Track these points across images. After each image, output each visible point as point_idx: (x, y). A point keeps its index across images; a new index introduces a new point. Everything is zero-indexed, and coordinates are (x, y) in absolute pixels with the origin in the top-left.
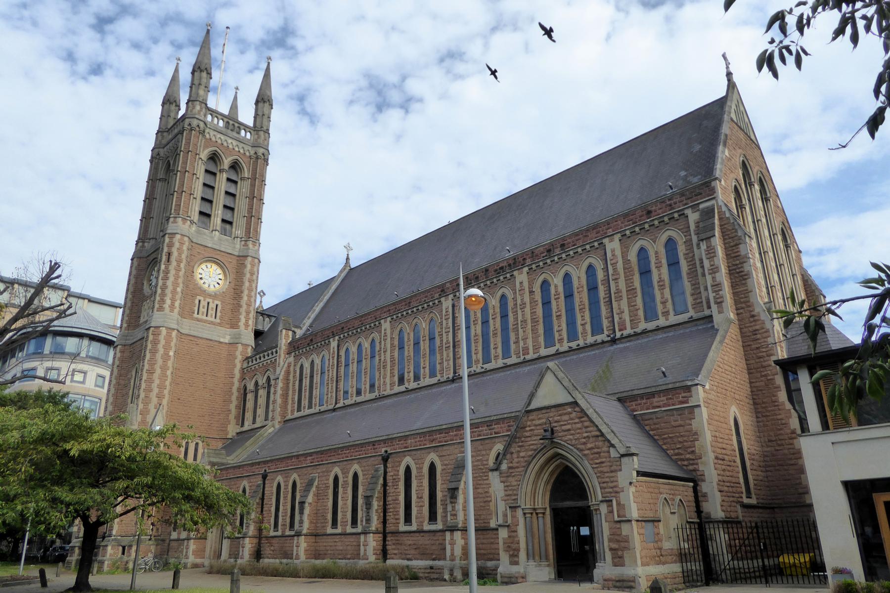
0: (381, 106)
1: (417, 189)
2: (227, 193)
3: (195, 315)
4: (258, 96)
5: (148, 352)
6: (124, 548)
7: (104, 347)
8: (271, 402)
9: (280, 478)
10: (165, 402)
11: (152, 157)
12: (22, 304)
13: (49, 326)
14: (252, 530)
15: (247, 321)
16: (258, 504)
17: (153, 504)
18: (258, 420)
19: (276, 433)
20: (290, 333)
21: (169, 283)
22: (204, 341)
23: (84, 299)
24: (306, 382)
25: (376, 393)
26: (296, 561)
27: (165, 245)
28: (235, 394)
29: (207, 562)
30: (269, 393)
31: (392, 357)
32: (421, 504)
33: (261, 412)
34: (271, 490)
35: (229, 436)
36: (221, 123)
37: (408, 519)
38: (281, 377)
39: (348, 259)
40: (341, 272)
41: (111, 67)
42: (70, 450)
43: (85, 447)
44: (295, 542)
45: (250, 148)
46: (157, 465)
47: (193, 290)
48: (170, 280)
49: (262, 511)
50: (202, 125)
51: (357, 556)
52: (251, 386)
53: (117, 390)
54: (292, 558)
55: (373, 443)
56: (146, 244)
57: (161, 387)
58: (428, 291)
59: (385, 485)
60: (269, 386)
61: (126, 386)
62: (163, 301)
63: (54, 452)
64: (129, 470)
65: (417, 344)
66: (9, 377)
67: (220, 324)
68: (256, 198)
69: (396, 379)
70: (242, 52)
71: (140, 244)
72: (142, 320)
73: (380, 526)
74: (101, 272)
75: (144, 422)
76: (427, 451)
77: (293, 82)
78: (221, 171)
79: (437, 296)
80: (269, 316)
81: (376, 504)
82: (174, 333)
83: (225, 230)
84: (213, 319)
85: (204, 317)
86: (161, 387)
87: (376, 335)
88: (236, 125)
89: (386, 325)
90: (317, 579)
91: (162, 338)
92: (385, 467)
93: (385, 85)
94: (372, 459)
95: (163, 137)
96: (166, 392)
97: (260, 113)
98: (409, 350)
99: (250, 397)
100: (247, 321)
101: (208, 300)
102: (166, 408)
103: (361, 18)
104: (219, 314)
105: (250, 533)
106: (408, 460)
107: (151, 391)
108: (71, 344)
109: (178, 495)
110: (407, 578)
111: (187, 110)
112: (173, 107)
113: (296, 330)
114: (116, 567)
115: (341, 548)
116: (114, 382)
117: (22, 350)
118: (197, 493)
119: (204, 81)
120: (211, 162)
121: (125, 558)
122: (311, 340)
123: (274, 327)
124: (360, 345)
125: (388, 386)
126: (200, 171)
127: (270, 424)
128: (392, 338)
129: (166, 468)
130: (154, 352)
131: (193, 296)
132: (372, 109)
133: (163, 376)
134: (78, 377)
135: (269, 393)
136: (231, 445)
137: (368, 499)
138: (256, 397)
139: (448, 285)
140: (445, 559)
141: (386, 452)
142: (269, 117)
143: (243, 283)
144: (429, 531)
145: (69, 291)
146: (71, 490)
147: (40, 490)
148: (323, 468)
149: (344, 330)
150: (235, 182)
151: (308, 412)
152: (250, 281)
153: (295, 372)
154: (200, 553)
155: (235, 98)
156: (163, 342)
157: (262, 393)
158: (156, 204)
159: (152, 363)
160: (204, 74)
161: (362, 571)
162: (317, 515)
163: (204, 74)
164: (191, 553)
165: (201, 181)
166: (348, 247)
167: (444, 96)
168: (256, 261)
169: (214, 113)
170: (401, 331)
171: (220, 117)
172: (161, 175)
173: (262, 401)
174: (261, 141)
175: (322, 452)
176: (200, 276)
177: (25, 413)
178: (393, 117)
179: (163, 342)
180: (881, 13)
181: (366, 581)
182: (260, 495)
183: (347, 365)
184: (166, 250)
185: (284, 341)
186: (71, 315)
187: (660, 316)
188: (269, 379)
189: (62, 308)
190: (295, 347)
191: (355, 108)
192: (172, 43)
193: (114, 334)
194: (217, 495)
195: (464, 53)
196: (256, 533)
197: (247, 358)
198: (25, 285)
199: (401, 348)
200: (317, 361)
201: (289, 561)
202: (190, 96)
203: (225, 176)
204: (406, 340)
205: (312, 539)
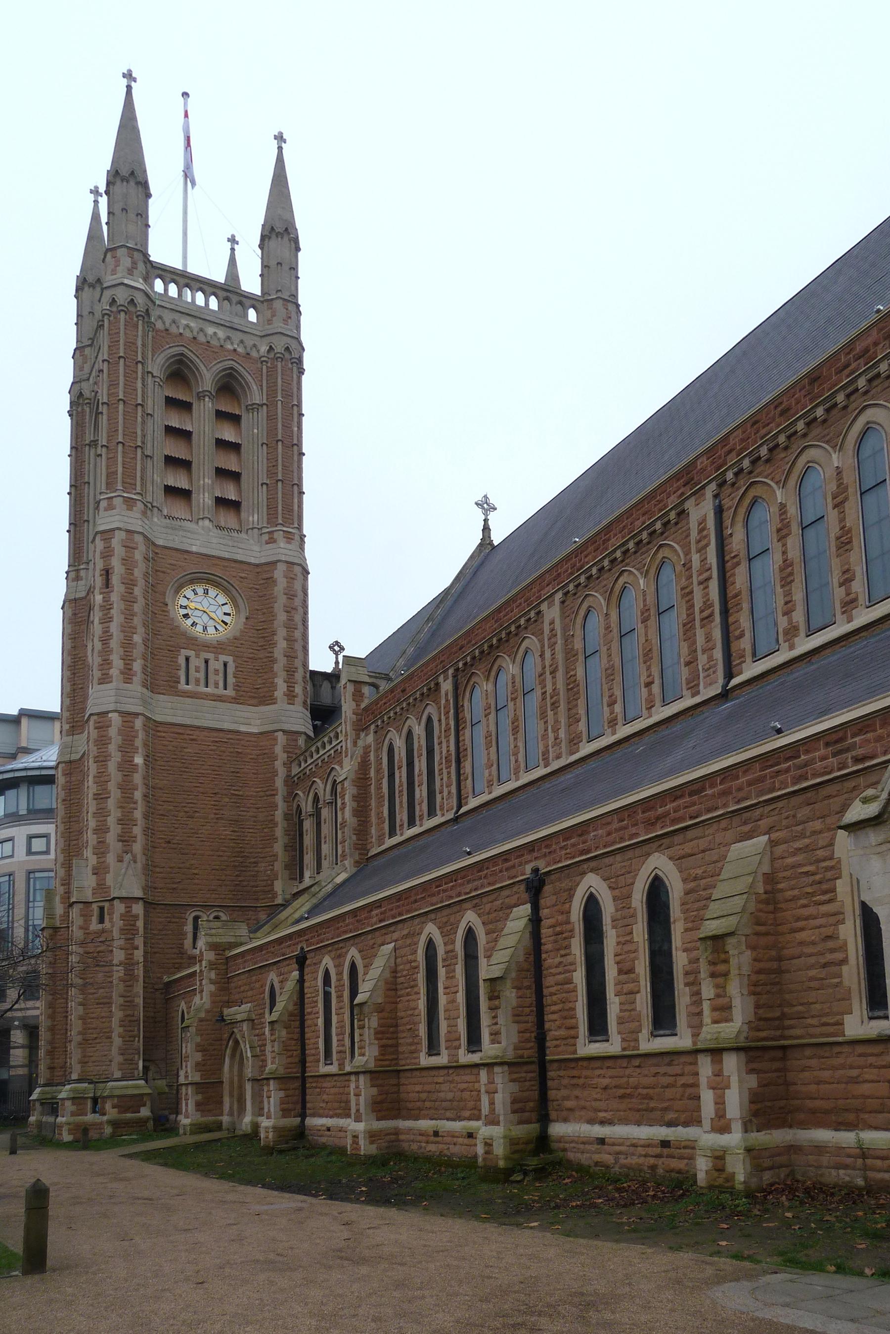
3: (183, 686)
24: (401, 776)
32: (627, 987)
37: (598, 1027)
39: (486, 529)
44: (353, 1086)
50: (140, 299)
52: (307, 807)
67: (235, 700)
78: (200, 397)
85: (202, 689)
96: (137, 831)
99: (308, 825)
102: (140, 858)
104: (231, 680)
106: (592, 882)
107: (120, 821)
115: (450, 1096)
131: (174, 650)
138: (319, 824)
140: (698, 1122)
141: (536, 871)
166: (486, 506)
168: (297, 569)
176: (184, 612)
180: (563, 1332)
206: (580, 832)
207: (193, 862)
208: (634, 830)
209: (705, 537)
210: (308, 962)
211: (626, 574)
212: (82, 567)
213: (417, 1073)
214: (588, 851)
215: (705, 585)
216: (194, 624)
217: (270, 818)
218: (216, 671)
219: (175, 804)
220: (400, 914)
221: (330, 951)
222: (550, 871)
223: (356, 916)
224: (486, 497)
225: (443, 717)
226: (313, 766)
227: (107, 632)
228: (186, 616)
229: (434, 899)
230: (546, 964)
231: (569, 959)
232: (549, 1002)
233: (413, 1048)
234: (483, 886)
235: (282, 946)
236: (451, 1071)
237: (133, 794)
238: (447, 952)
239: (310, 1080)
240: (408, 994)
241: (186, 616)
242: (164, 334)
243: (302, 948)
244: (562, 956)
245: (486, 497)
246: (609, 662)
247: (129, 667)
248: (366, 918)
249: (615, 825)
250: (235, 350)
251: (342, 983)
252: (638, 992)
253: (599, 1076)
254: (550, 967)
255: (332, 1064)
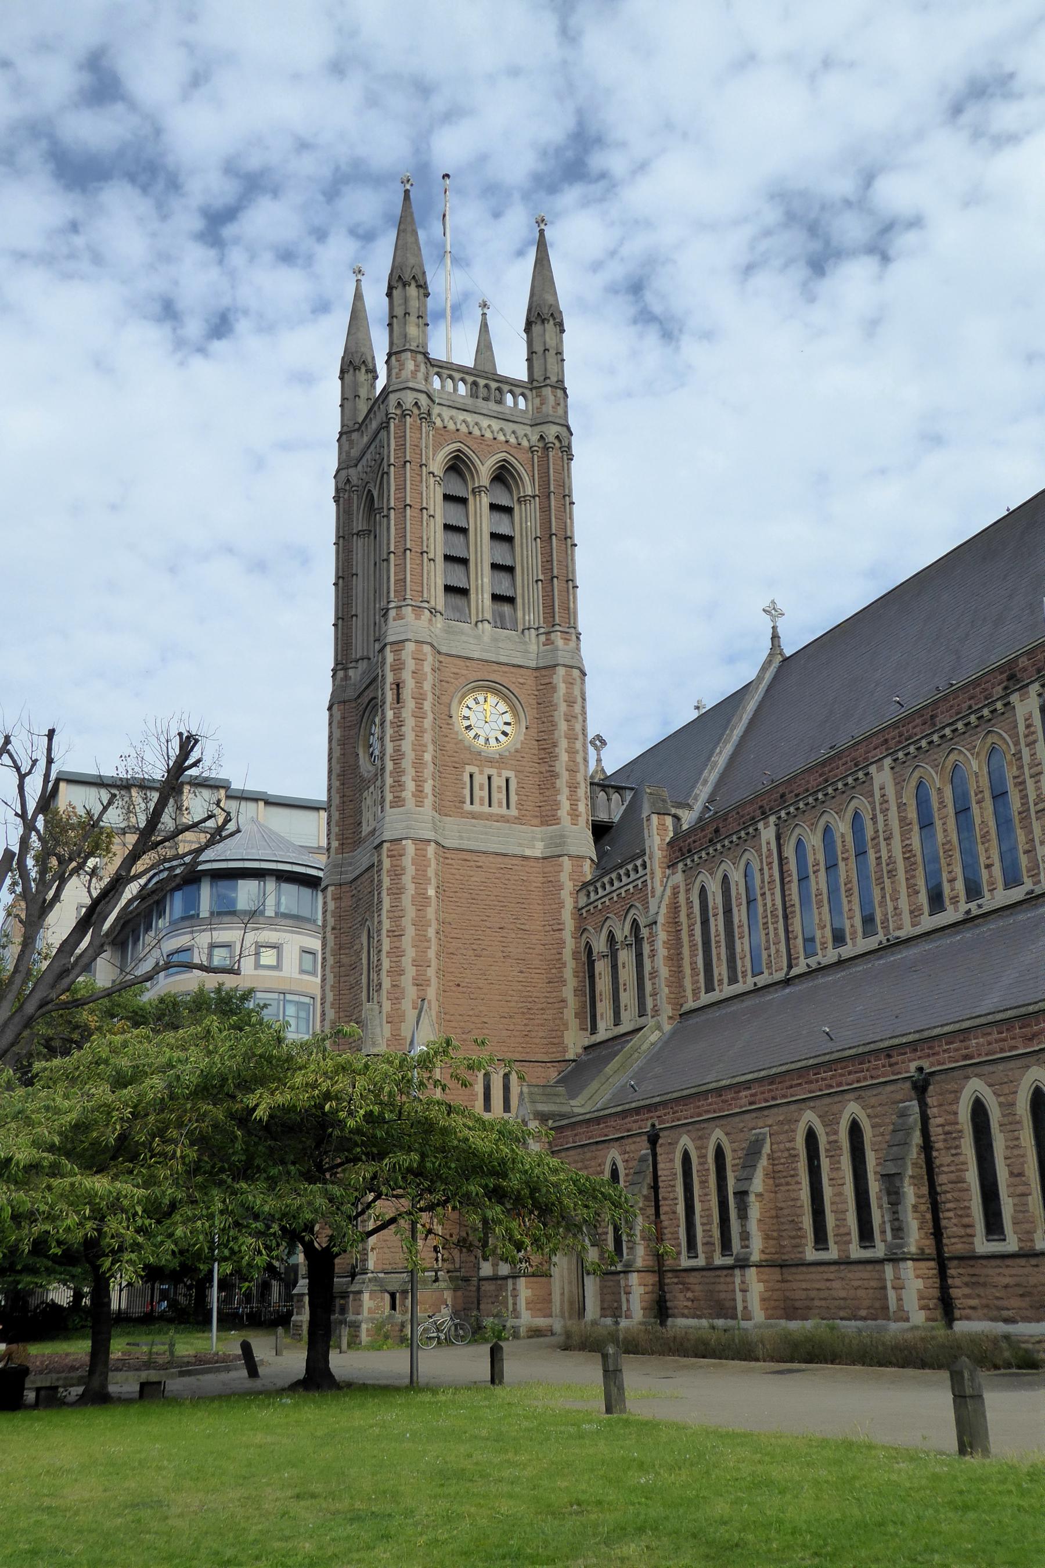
0: (819, 265)
1: (934, 440)
2: (494, 536)
3: (467, 806)
4: (529, 310)
5: (384, 893)
6: (393, 1296)
7: (306, 892)
8: (647, 976)
9: (685, 1141)
10: (431, 993)
11: (337, 490)
12: (142, 825)
13: (195, 863)
14: (641, 1255)
15: (574, 805)
16: (646, 1198)
17: (430, 1208)
18: (625, 1015)
19: (666, 1043)
20: (669, 821)
21: (407, 746)
22: (491, 859)
23: (256, 800)
24: (717, 925)
25: (881, 937)
26: (744, 1324)
27: (388, 667)
28: (570, 965)
29: (558, 1326)
30: (639, 955)
31: (907, 849)
32: (1021, 1189)
33: (628, 997)
34: (670, 1167)
35: (570, 1056)
36: (462, 389)
38: (661, 920)
39: (775, 637)
40: (764, 669)
41: (246, 312)
42: (254, 1109)
43: (280, 1099)
44: (738, 1280)
45: (528, 430)
46: (427, 1127)
47: (455, 755)
48: (408, 738)
49: (657, 1214)
50: (423, 400)
51: (882, 1311)
52: (600, 945)
53: (338, 976)
54: (734, 1317)
55: (888, 1052)
56: (351, 672)
57: (420, 964)
58: (975, 683)
59: (927, 1147)
60: (639, 940)
61: (354, 967)
62: (399, 785)
63: (231, 1115)
64: (373, 1140)
65: (963, 811)
66: (146, 967)
67: (519, 820)
68: (557, 537)
69: (923, 898)
70: (497, 215)
71: (341, 674)
72: (366, 829)
73: (929, 1244)
74: (274, 742)
75: (396, 1037)
76: (1019, 1063)
77: (613, 254)
79: (998, 691)
80: (618, 789)
81: (911, 1193)
82: (431, 849)
83: (502, 616)
84: (504, 811)
85: (486, 809)
86: (420, 964)
87: (860, 802)
88: (494, 385)
89: (882, 777)
90: (796, 1366)
91: (407, 861)
92: (923, 1105)
93: (823, 208)
94: (889, 1088)
95: (351, 442)
96: (431, 972)
97: (538, 348)
98: (946, 828)
99: (602, 967)
100: (574, 805)
101: (489, 771)
102: (435, 1005)
103: (747, 61)
104: (513, 798)
105: (639, 1263)
106: (975, 1086)
107: (401, 972)
108: (246, 892)
109: (474, 1188)
110: (1009, 1366)
111: (389, 376)
112: (362, 376)
113: (679, 812)
114: (383, 1337)
116: (330, 961)
117: (161, 914)
118: (514, 1182)
119: (414, 304)
120: (453, 477)
121: (398, 1317)
122: (717, 831)
123: (632, 810)
124: (827, 830)
125: (906, 918)
126: (444, 498)
127: (652, 1022)
128: (901, 806)
129: (445, 1131)
130: (397, 892)
131: (458, 767)
132: (800, 272)
133: (421, 939)
134: (268, 957)
135: (639, 955)
136: (577, 1073)
137: (892, 1183)
138: (614, 967)
139: (1023, 662)
141: (920, 1069)
142: (559, 353)
143: (554, 724)
144: (685, 1270)
145: (227, 788)
146: (271, 1188)
147: (215, 1192)
148: (779, 1115)
149: (788, 799)
150: (508, 510)
151: (729, 990)
152: (570, 718)
153: (689, 903)
154: (542, 1304)
155: (484, 327)
156: (410, 870)
157: (626, 956)
158: (359, 585)
159: (397, 917)
160: (412, 291)
161: (896, 1348)
162: (779, 1221)
163: (412, 291)
164: (523, 1305)
165: (440, 521)
166: (772, 611)
167: (972, 199)
168: (576, 673)
169: (446, 369)
170: (920, 785)
171: (457, 376)
172: (359, 524)
173: (627, 975)
174: (548, 409)
175: (771, 1079)
176: (466, 723)
177: (170, 1036)
178: (854, 282)
179: (410, 870)
181: (910, 1372)
182: (649, 1180)
183: (803, 879)
184: (390, 678)
185: (657, 840)
186: (232, 835)
187: (1026, 879)
188: (635, 925)
189: (211, 824)
190: (683, 849)
191: (762, 280)
192: (353, 232)
193: (317, 864)
194: (555, 1185)
195: (1011, 76)
196: (651, 1262)
197: (585, 885)
198: (144, 785)
199: (926, 824)
200: (736, 876)
201: (731, 1323)
202: (391, 344)
203: (485, 500)
204: (935, 805)
205: (775, 1274)
206: (962, 1038)
207: (481, 1008)
208: (1013, 1043)
209: (1033, 733)
210: (660, 1141)
211: (956, 752)
212: (351, 665)
213: (804, 1269)
214: (972, 1058)
215: (1037, 778)
216: (477, 736)
217: (558, 956)
218: (499, 787)
219: (464, 941)
220: (774, 1098)
221: (689, 1131)
222: (934, 1072)
223: (721, 1096)
224: (773, 602)
225: (766, 868)
226: (606, 899)
227: (399, 750)
228: (469, 728)
229: (813, 1086)
230: (937, 1162)
231: (962, 1158)
232: (943, 1199)
233: (798, 1240)
234: (865, 1079)
235: (626, 1121)
236: (842, 1267)
237: (426, 931)
238: (829, 1143)
239: (669, 1275)
240: (788, 1184)
241: (469, 728)
242: (442, 432)
243: (653, 1125)
244: (953, 1155)
245: (773, 602)
246: (945, 837)
247: (420, 789)
248: (733, 1099)
249: (995, 1036)
250: (507, 442)
251: (706, 1167)
252: (1030, 1194)
253: (999, 1274)
254: (941, 1165)
255: (696, 1257)
